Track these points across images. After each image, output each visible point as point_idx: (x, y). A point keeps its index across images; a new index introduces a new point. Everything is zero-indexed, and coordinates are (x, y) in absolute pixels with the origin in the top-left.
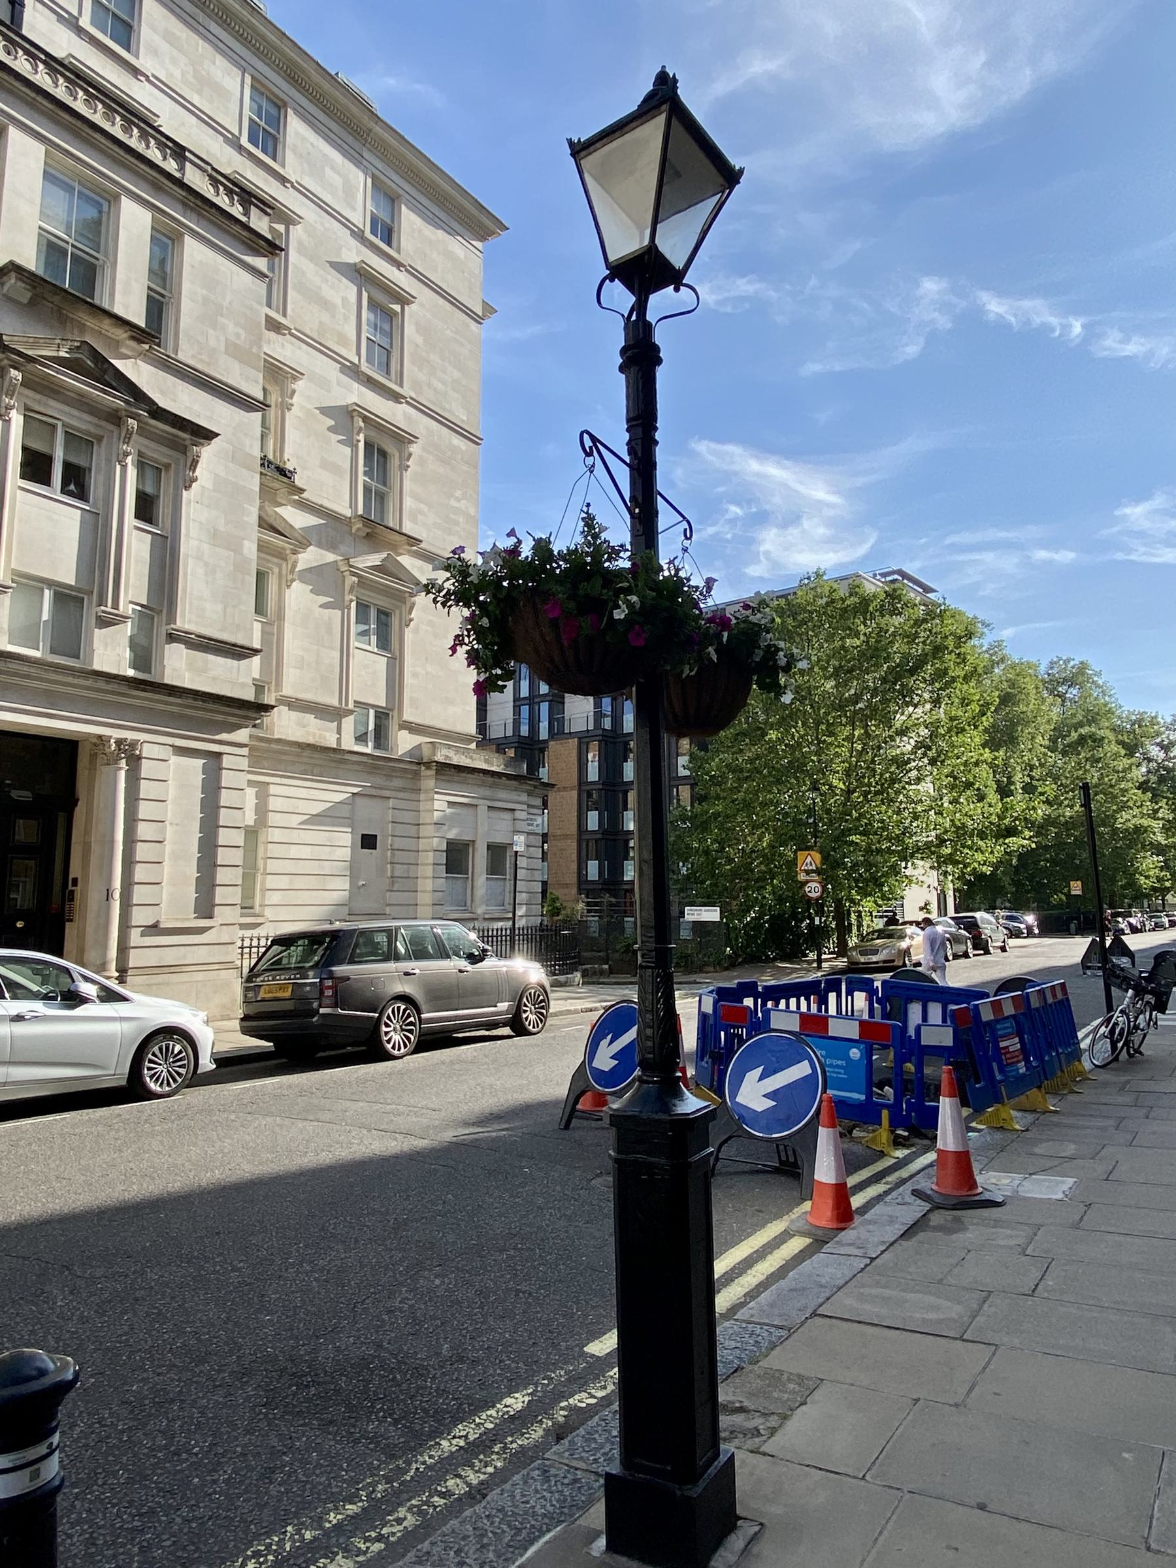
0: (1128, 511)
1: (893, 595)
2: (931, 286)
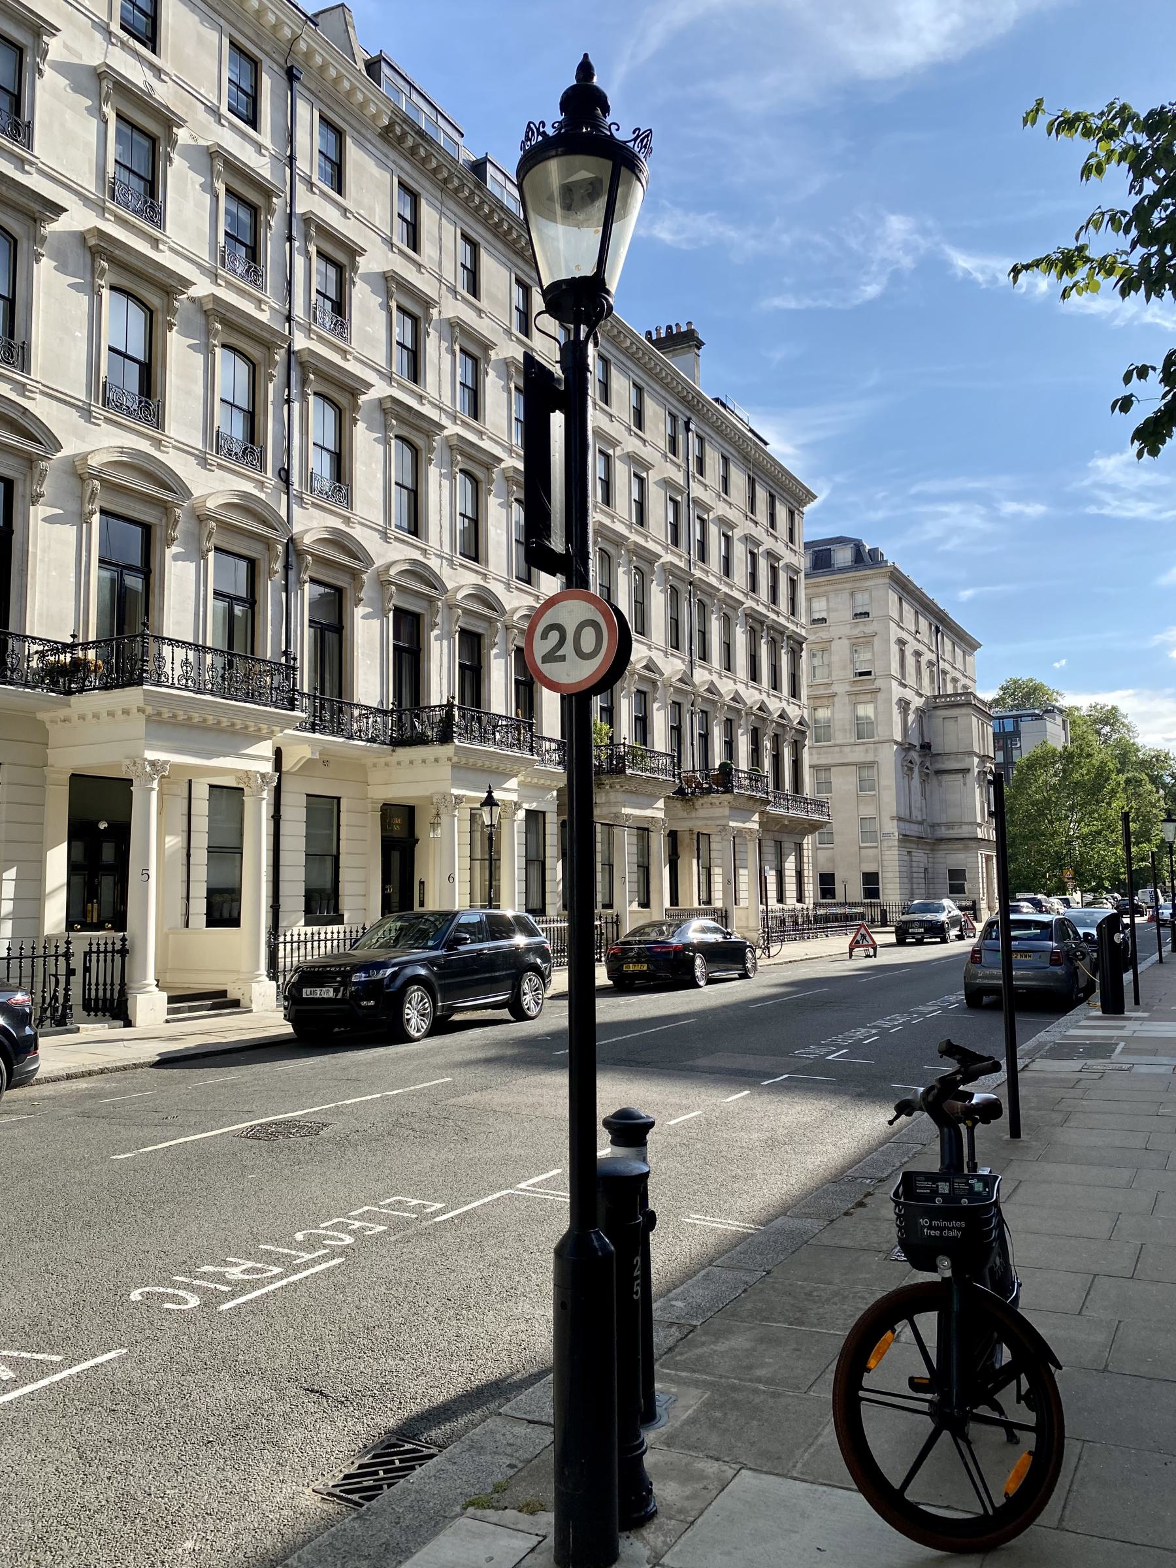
0: (1100, 463)
2: (897, 225)
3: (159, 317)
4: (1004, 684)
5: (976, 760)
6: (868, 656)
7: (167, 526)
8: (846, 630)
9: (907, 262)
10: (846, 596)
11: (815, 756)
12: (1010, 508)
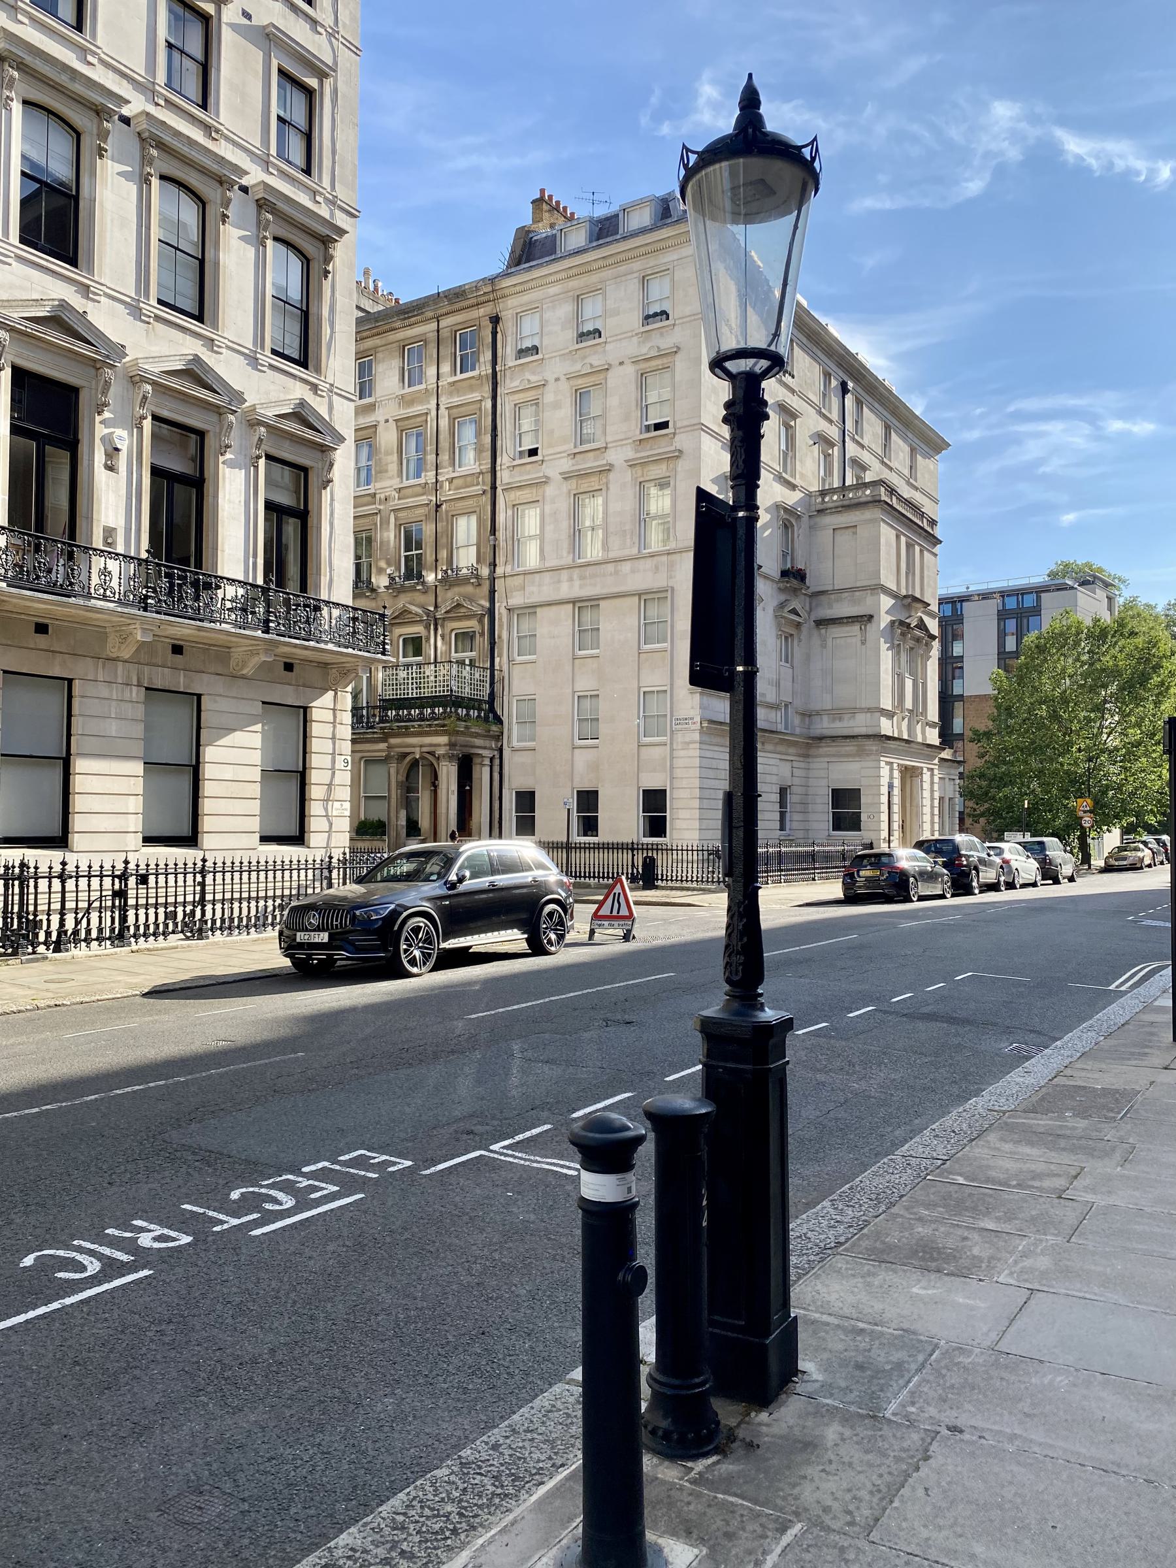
1: (1121, 624)
2: (1003, 111)
3: (314, 266)
4: (1053, 567)
5: (886, 602)
6: (666, 394)
7: (220, 433)
8: (632, 348)
9: (1014, 154)
10: (634, 285)
11: (577, 583)
12: (1116, 426)
